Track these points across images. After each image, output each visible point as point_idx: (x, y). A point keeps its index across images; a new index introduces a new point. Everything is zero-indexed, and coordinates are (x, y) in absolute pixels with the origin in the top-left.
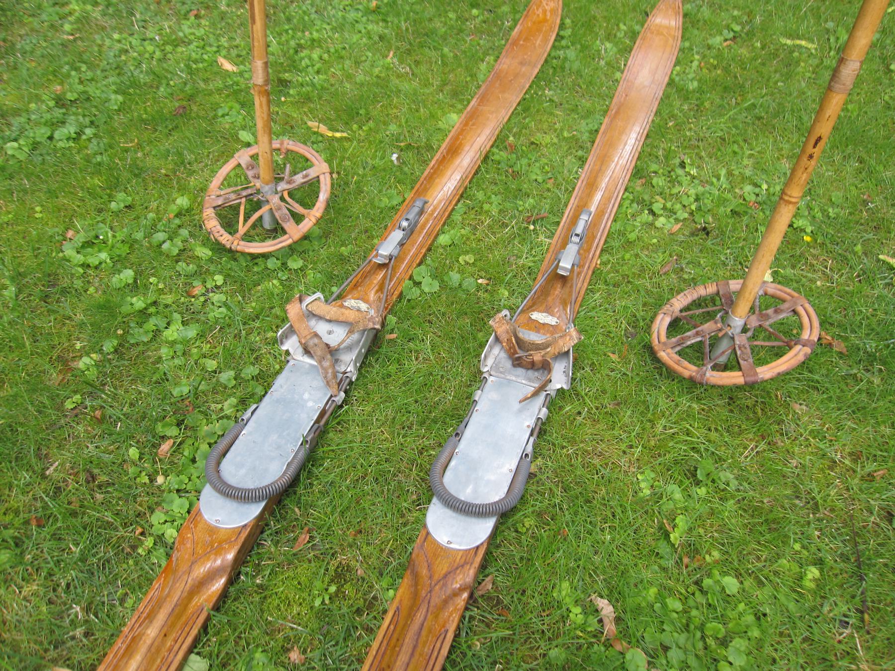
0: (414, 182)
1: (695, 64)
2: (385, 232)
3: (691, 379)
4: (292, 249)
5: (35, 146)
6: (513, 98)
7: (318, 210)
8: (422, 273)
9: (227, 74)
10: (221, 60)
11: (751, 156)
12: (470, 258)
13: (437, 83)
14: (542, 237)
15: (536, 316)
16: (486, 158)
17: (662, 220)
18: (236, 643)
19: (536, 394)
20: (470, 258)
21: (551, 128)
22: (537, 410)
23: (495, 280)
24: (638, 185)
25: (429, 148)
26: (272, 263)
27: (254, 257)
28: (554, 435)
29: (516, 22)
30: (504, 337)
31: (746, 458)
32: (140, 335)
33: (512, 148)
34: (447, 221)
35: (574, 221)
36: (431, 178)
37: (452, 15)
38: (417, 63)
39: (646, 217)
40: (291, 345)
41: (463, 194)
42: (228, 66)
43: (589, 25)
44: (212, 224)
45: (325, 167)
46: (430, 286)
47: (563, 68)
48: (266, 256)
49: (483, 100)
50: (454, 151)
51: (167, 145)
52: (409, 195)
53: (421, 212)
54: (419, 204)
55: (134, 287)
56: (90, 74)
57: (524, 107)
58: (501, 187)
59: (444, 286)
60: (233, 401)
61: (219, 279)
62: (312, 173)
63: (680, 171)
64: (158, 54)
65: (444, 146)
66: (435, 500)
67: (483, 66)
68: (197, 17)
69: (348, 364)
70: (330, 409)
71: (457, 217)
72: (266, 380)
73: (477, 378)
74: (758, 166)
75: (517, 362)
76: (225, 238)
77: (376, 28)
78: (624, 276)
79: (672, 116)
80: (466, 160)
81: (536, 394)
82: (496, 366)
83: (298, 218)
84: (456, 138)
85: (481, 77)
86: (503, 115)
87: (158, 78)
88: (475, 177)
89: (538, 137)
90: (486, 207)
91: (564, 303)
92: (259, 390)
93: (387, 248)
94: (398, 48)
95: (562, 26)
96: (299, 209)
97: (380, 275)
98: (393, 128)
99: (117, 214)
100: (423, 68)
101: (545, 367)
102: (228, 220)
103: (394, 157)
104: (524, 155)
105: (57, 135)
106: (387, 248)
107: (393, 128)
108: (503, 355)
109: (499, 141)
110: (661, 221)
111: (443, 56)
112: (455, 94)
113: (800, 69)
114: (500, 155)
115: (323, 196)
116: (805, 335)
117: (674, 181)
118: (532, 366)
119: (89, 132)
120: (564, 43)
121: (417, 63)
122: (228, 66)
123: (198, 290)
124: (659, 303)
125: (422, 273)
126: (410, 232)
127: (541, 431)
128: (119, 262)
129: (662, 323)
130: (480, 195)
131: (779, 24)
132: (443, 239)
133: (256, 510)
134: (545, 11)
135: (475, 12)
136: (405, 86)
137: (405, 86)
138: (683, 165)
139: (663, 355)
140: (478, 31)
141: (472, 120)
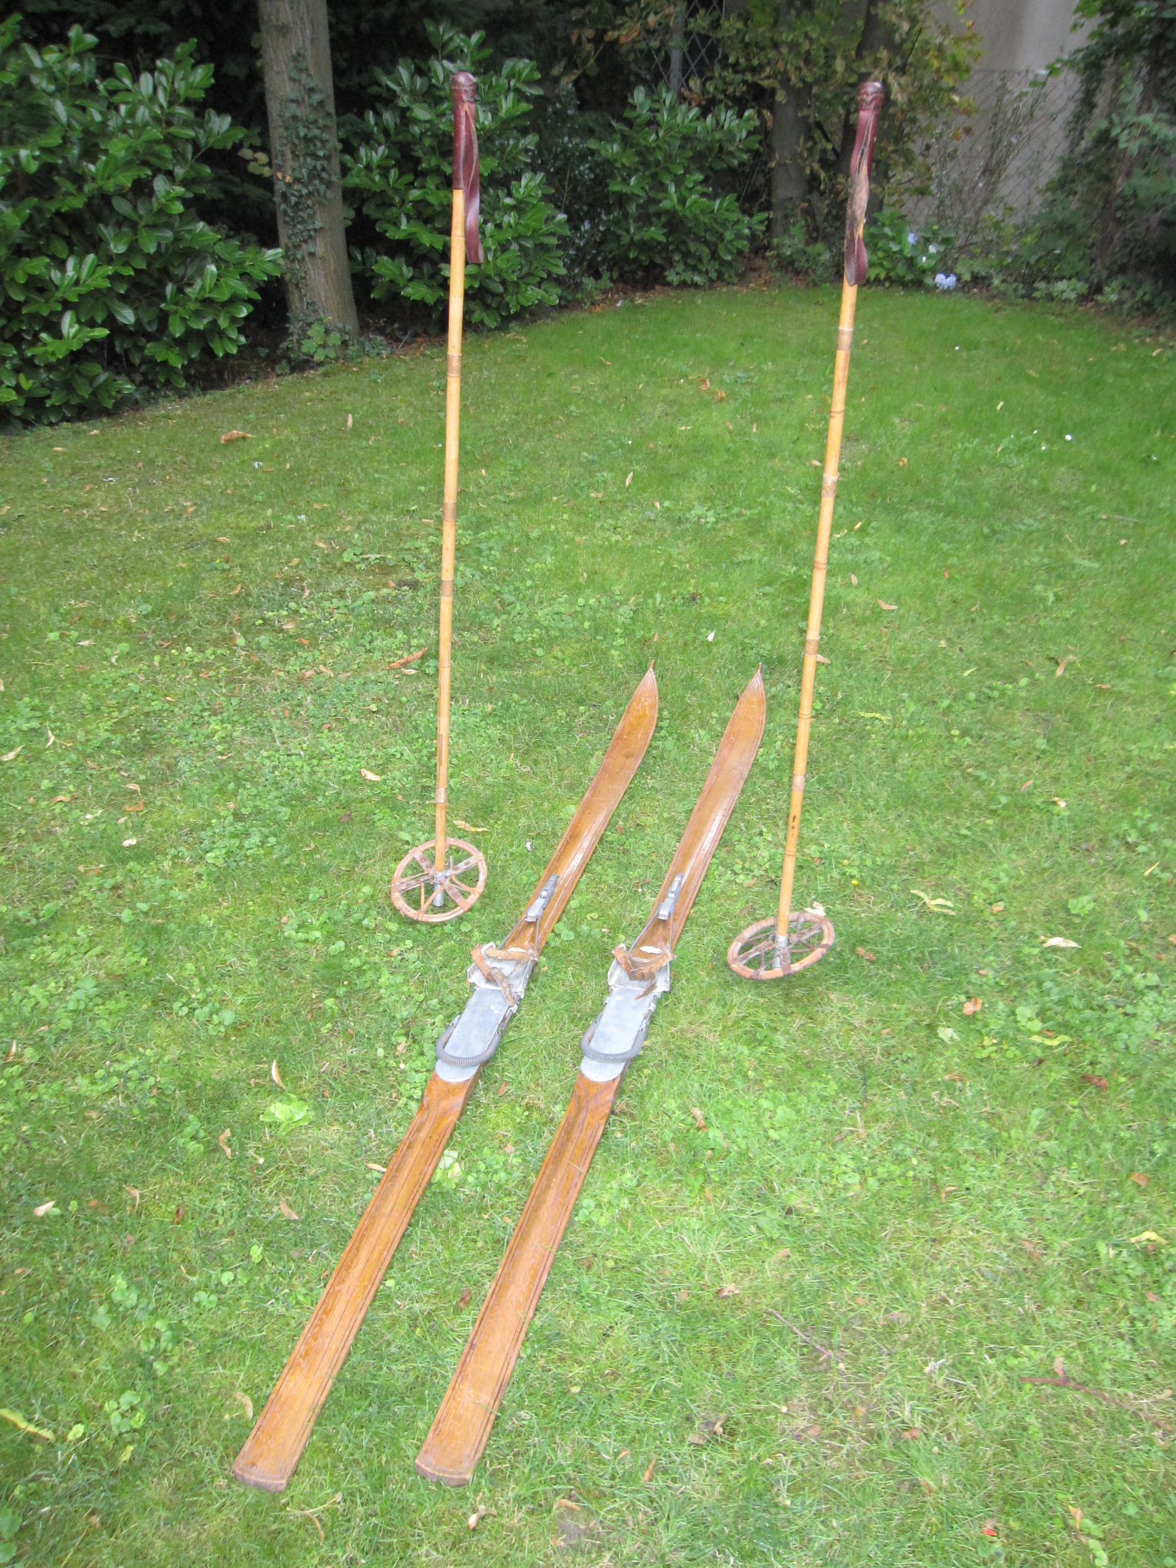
0: (546, 862)
1: (778, 744)
2: (529, 901)
3: (751, 978)
4: (461, 919)
5: (229, 853)
6: (621, 788)
7: (480, 887)
8: (562, 928)
9: (372, 785)
10: (364, 772)
11: (819, 822)
12: (595, 915)
13: (555, 779)
14: (648, 897)
15: (645, 949)
16: (601, 841)
17: (742, 877)
18: (462, 1260)
19: (645, 994)
20: (595, 915)
21: (654, 812)
22: (649, 1004)
23: (615, 930)
24: (723, 854)
25: (555, 835)
26: (448, 929)
27: (433, 926)
28: (660, 1020)
29: (619, 717)
30: (622, 961)
31: (794, 1028)
32: (360, 983)
33: (623, 831)
34: (575, 889)
35: (671, 883)
36: (559, 858)
37: (560, 712)
38: (536, 762)
39: (729, 875)
40: (476, 978)
41: (585, 869)
42: (371, 776)
43: (685, 715)
44: (400, 903)
45: (481, 855)
46: (567, 935)
47: (662, 758)
48: (444, 923)
49: (595, 790)
50: (574, 836)
51: (340, 845)
52: (543, 873)
53: (555, 885)
54: (553, 879)
55: (346, 953)
56: (254, 791)
57: (630, 795)
58: (614, 862)
59: (578, 935)
60: (441, 1017)
61: (409, 943)
62: (472, 861)
63: (757, 839)
64: (307, 769)
65: (566, 832)
66: (212, 66)
67: (593, 761)
68: (330, 729)
69: (519, 988)
70: (508, 1015)
71: (582, 887)
72: (461, 1005)
73: (607, 990)
74: (826, 830)
75: (633, 976)
76: (412, 913)
77: (494, 732)
78: (712, 920)
79: (754, 794)
80: (586, 842)
81: (645, 994)
82: (619, 982)
83: (465, 895)
84: (576, 826)
85: (592, 770)
86: (613, 803)
87: (314, 790)
88: (593, 856)
89: (643, 820)
90: (604, 878)
91: (665, 940)
92: (457, 1010)
93: (533, 912)
94: (517, 749)
95: (661, 719)
96: (465, 888)
97: (531, 930)
98: (523, 821)
99: (314, 903)
100: (542, 767)
101: (652, 976)
102: (413, 899)
103: (528, 845)
104: (632, 835)
105: (246, 844)
106: (533, 912)
107: (523, 821)
108: (624, 974)
109: (611, 825)
110: (741, 878)
111: (558, 755)
112: (571, 787)
113: (871, 742)
114: (612, 836)
115: (482, 877)
116: (825, 942)
117: (753, 846)
118: (643, 977)
119: (272, 840)
120: (663, 733)
121: (536, 762)
122: (371, 776)
123: (396, 952)
124: (735, 932)
125: (562, 928)
126: (549, 899)
127: (652, 1018)
128: (330, 938)
129: (736, 946)
130: (599, 869)
131: (857, 698)
132: (574, 904)
133: (472, 1072)
134: (644, 708)
135: (582, 708)
136: (528, 784)
137: (528, 784)
138: (761, 834)
139: (734, 966)
140: (584, 730)
141: (586, 810)
